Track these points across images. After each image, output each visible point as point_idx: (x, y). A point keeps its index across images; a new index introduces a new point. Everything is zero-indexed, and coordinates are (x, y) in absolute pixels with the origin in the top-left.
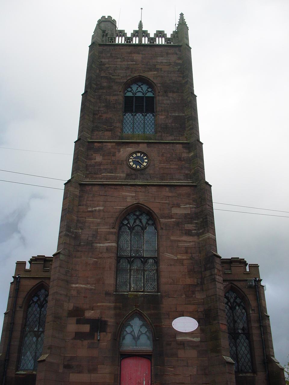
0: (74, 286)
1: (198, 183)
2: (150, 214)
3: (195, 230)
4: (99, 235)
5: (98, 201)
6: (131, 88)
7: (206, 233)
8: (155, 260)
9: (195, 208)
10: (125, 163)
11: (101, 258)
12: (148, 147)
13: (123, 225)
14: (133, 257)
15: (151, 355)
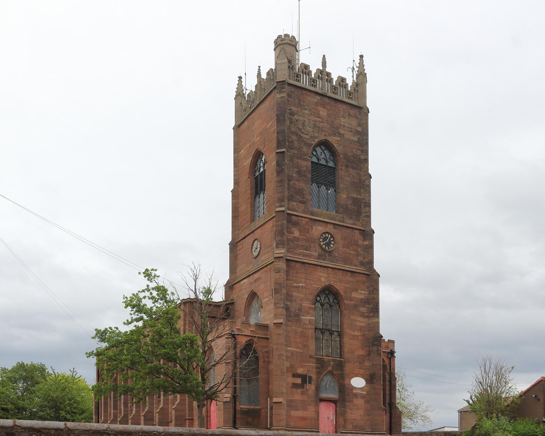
3: (367, 313)
8: (338, 333)
11: (305, 328)
12: (334, 228)
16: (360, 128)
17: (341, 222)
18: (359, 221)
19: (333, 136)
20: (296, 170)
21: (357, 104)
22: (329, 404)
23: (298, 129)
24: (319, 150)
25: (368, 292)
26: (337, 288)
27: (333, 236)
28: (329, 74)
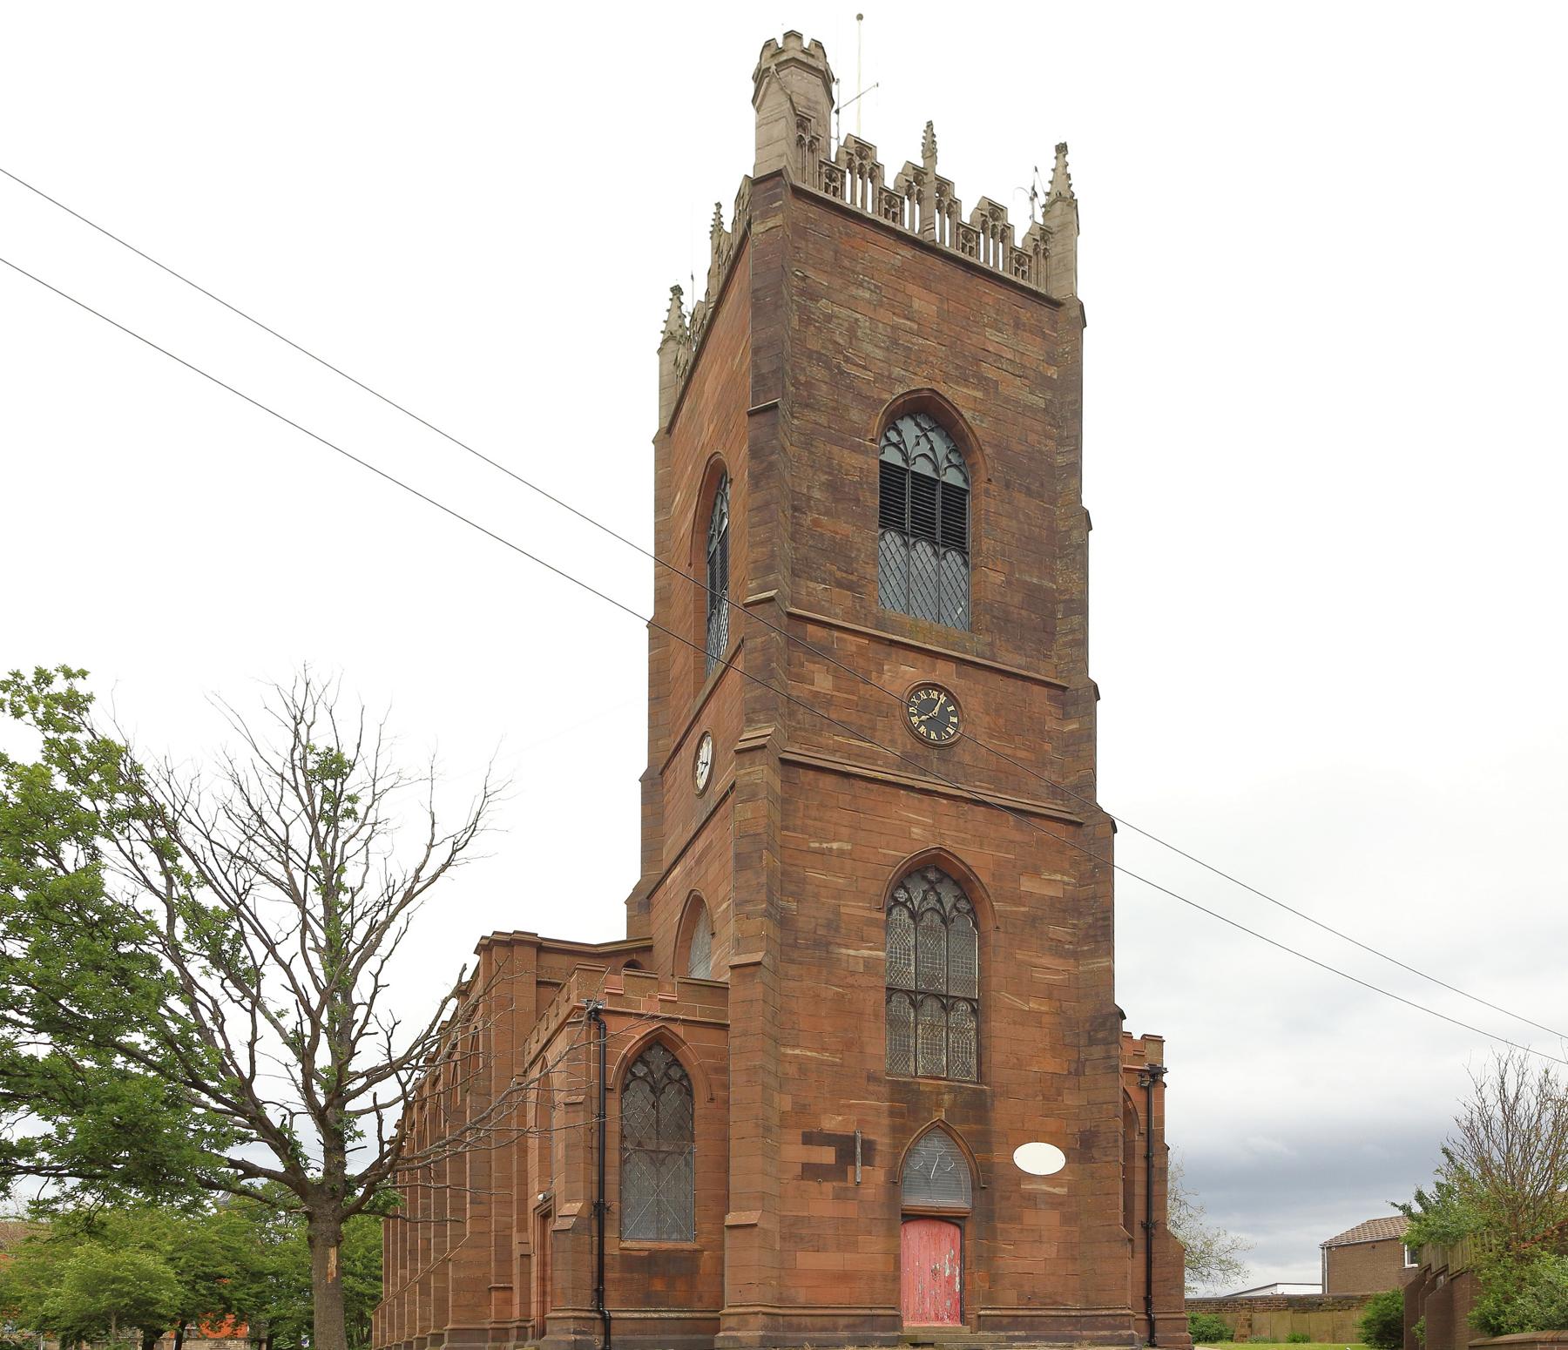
4: (843, 925)
5: (835, 824)
7: (1101, 956)
9: (1074, 885)
12: (959, 675)
13: (897, 902)
14: (921, 993)
19: (957, 383)
20: (824, 478)
24: (909, 429)
28: (944, 186)
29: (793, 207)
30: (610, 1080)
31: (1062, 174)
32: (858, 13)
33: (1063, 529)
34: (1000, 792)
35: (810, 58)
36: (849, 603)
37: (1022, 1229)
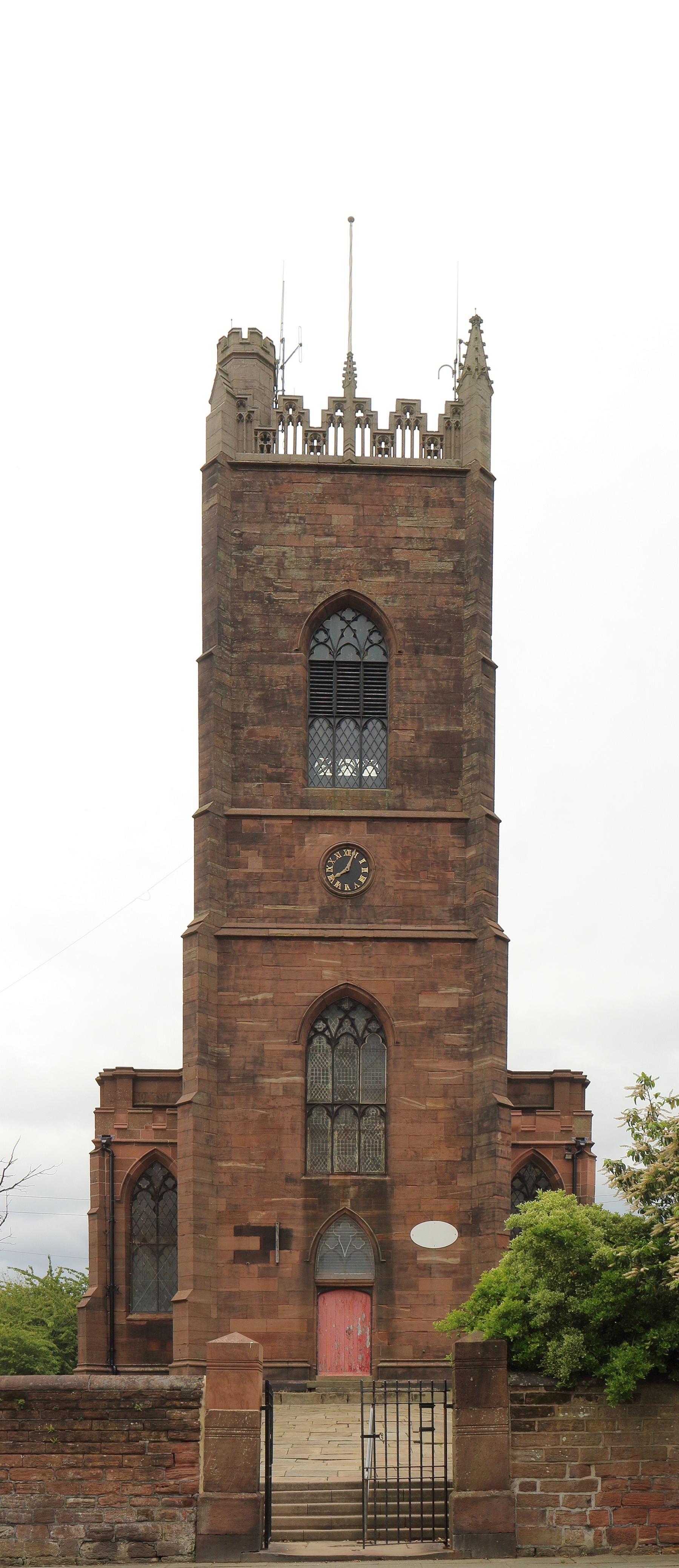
0: (224, 1164)
1: (481, 933)
2: (371, 1009)
3: (466, 1045)
4: (266, 1060)
6: (326, 632)
8: (381, 1110)
10: (316, 876)
11: (274, 1108)
12: (370, 831)
13: (317, 1033)
15: (370, 1287)
16: (463, 530)
17: (394, 809)
18: (455, 796)
19: (372, 575)
20: (257, 694)
21: (455, 467)
22: (351, 1297)
23: (262, 583)
25: (470, 989)
26: (372, 990)
27: (366, 853)
28: (363, 404)
29: (232, 479)
30: (118, 1194)
31: (476, 344)
32: (350, 215)
33: (468, 676)
34: (406, 923)
35: (247, 346)
36: (278, 792)
37: (417, 1295)
